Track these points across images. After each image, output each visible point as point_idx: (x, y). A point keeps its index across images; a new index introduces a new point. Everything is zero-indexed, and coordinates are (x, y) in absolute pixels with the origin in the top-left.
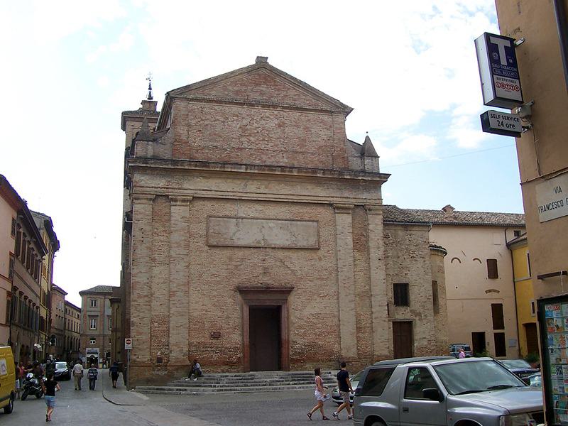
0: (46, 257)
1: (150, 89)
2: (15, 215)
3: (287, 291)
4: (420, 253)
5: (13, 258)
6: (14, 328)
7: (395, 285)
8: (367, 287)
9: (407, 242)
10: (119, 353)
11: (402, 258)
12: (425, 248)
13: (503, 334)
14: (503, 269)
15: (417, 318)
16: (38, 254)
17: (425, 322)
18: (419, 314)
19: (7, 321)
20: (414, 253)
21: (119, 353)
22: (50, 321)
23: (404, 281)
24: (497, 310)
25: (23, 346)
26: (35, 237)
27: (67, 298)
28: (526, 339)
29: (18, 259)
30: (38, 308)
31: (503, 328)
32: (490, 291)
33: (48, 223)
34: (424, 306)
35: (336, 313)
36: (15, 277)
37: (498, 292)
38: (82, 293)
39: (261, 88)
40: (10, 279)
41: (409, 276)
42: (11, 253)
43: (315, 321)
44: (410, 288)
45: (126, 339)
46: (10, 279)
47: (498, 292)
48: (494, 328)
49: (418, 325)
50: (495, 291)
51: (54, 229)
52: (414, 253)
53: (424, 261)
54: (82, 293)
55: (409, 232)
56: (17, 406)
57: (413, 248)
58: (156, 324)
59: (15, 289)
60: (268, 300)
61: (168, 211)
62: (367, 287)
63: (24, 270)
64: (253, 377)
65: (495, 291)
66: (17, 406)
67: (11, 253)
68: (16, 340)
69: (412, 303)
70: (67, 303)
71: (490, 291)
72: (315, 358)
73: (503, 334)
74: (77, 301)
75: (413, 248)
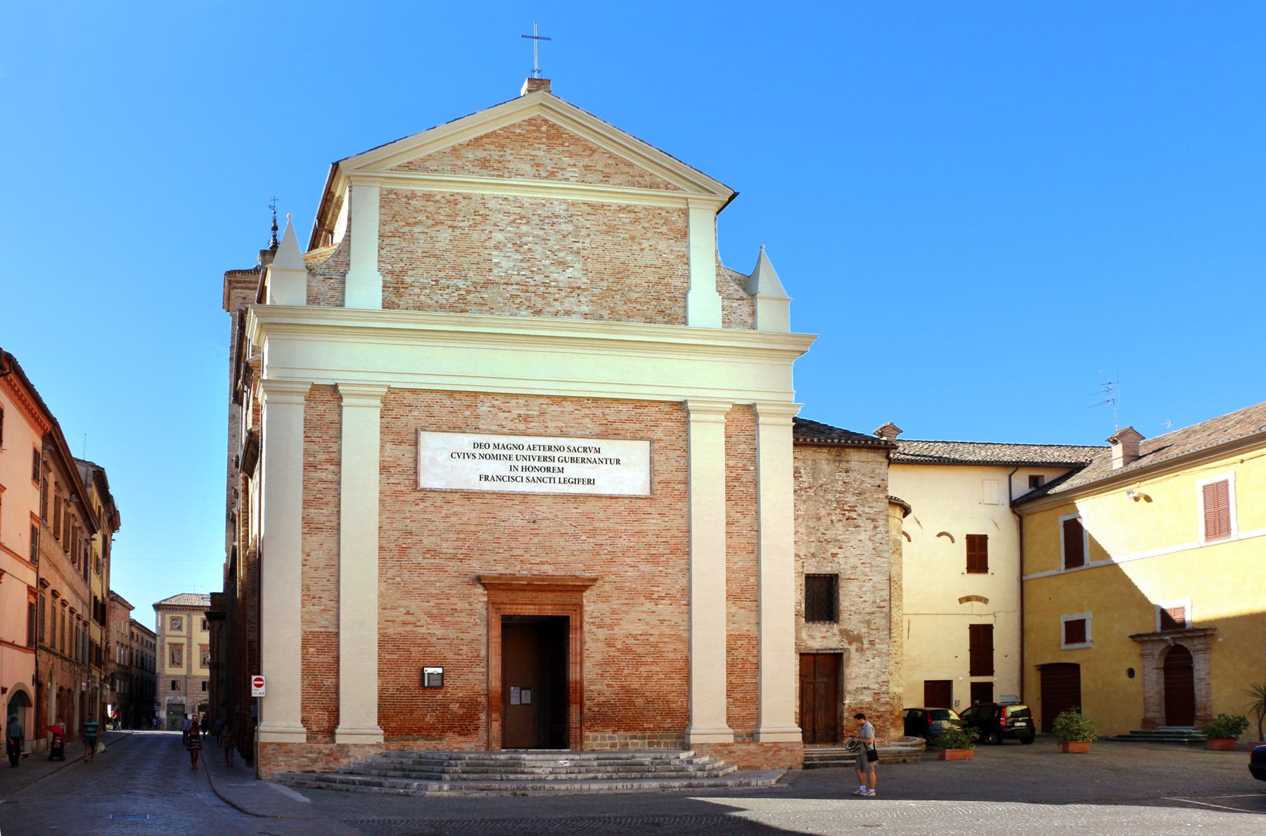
0: (98, 537)
1: (275, 228)
2: (39, 443)
3: (576, 588)
4: (867, 510)
5: (37, 525)
6: (44, 656)
7: (810, 578)
8: (752, 580)
9: (839, 486)
10: (223, 705)
11: (826, 521)
12: (877, 500)
13: (990, 685)
14: (1001, 553)
15: (853, 648)
16: (85, 529)
17: (868, 654)
18: (857, 639)
19: (30, 641)
20: (852, 509)
21: (223, 705)
22: (108, 650)
23: (827, 569)
24: (981, 637)
25: (61, 689)
26: (81, 503)
27: (134, 615)
28: (1039, 695)
29: (47, 528)
30: (86, 624)
31: (991, 673)
32: (968, 599)
33: (100, 476)
34: (868, 622)
35: (685, 635)
36: (42, 561)
37: (985, 601)
38: (157, 607)
39: (534, 153)
40: (34, 561)
41: (840, 559)
42: (32, 514)
43: (640, 650)
44: (841, 584)
45: (254, 677)
46: (34, 561)
47: (985, 601)
48: (973, 673)
49: (854, 662)
50: (979, 599)
51: (111, 491)
52: (852, 509)
53: (875, 527)
54: (157, 607)
55: (844, 465)
56: (256, 261)
57: (851, 499)
58: (312, 650)
59: (42, 583)
60: (547, 607)
61: (336, 418)
62: (752, 580)
63: (61, 552)
64: (515, 766)
65: (979, 599)
66: (256, 261)
67: (32, 514)
68: (47, 677)
69: (844, 616)
70: (133, 623)
71: (968, 599)
72: (1224, 734)
73: (990, 685)
74: (146, 617)
75: (851, 499)
